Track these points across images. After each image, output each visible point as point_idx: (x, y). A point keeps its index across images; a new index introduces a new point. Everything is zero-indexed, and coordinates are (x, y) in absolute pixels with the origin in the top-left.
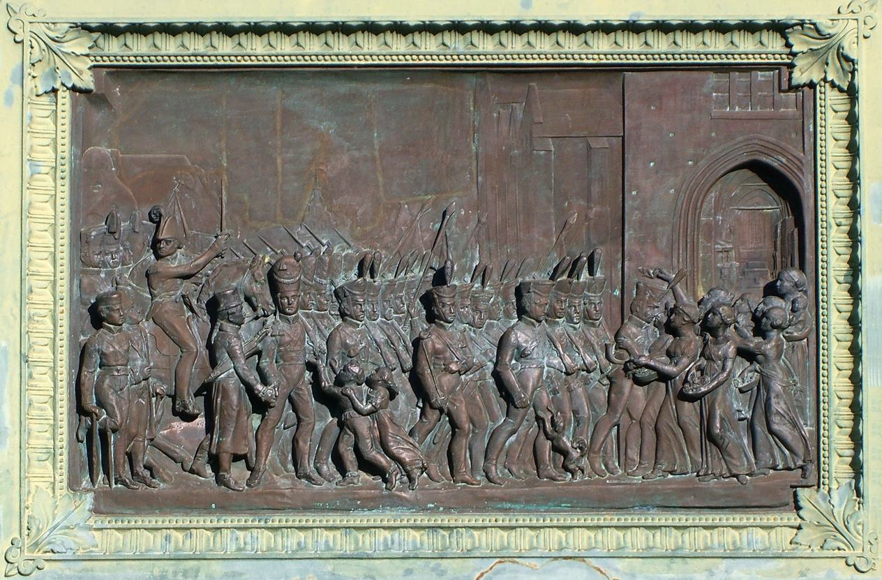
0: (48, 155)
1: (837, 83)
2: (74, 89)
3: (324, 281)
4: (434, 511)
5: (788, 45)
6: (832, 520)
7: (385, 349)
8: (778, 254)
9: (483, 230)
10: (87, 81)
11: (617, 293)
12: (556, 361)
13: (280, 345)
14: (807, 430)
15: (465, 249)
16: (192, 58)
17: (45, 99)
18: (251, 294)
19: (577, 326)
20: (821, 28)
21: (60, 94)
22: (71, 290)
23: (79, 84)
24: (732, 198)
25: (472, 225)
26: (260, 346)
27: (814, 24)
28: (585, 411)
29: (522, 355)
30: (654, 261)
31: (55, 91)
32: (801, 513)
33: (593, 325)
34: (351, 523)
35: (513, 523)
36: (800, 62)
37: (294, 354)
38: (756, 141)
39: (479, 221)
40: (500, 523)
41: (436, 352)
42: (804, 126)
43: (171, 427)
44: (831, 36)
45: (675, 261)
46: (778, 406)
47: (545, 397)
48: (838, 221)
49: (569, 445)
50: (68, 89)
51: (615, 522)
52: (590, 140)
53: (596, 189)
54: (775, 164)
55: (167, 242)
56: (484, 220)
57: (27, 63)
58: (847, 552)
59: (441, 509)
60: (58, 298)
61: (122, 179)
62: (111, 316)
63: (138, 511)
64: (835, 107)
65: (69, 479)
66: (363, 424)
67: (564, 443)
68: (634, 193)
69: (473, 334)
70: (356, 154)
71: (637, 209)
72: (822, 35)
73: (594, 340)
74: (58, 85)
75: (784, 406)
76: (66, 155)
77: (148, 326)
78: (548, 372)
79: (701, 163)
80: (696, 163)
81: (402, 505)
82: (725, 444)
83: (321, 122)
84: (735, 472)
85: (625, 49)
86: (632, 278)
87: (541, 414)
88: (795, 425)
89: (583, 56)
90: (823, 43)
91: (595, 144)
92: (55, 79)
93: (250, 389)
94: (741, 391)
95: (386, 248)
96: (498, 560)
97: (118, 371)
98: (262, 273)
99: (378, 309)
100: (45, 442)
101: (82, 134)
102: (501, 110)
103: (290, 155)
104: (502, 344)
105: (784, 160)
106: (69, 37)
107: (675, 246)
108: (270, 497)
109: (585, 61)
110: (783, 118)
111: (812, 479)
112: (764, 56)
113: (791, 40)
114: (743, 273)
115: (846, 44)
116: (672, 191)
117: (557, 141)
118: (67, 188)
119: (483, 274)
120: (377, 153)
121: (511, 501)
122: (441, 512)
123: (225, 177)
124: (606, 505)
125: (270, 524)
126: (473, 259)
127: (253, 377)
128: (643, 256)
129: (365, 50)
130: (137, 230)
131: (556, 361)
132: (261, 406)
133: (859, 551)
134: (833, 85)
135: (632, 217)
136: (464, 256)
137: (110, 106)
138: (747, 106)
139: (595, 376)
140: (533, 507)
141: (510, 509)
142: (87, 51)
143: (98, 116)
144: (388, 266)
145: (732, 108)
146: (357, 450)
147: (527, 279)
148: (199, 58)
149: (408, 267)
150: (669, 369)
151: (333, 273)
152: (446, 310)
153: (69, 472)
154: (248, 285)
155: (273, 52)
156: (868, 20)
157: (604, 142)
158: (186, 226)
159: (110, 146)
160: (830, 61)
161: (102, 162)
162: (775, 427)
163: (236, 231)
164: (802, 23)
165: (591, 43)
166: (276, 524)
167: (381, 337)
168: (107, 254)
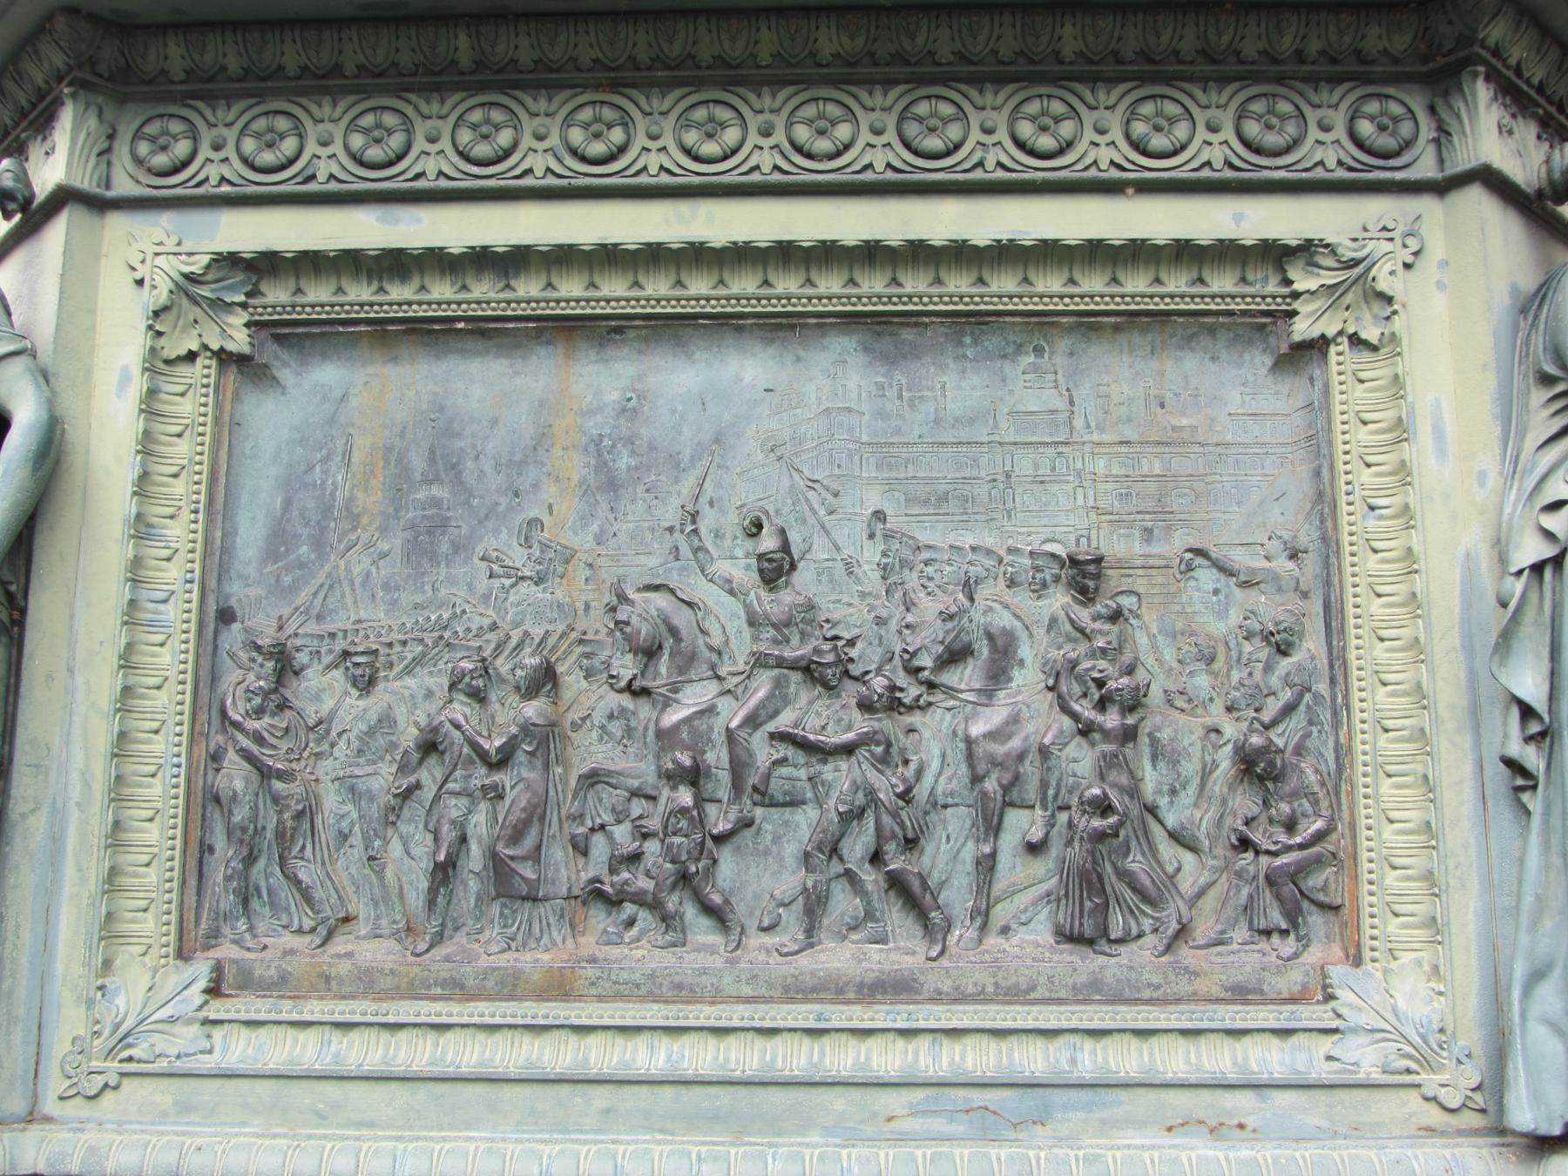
133: (1444, 1077)
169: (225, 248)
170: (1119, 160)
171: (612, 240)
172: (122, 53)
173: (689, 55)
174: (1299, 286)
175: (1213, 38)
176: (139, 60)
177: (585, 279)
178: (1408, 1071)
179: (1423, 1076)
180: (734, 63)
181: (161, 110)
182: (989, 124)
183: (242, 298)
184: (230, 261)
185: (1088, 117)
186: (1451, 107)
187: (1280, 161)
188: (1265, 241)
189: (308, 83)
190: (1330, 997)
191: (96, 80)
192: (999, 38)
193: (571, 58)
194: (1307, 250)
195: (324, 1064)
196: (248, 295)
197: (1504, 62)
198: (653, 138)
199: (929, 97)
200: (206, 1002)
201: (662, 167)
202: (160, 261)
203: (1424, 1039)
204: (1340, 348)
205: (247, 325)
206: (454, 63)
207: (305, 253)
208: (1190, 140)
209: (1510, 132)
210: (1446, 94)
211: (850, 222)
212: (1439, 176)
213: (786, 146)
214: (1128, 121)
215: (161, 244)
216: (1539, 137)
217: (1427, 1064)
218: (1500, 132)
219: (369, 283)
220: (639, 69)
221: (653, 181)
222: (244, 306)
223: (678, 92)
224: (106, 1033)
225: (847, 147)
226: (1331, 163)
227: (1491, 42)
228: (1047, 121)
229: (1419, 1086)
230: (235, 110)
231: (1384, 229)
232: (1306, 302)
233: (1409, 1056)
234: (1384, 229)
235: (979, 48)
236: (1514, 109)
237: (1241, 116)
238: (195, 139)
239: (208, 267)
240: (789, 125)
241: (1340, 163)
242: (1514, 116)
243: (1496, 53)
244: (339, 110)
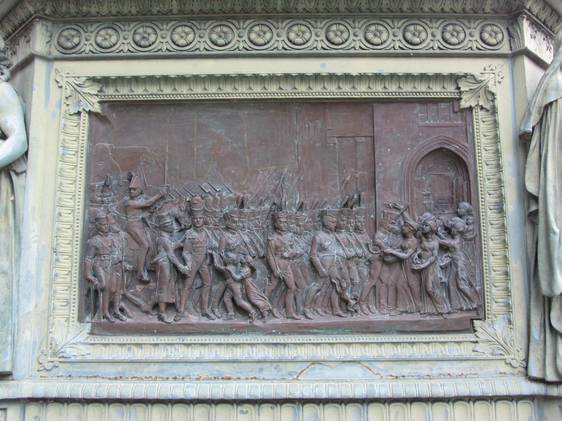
0: (74, 146)
1: (484, 106)
2: (90, 113)
3: (217, 210)
4: (276, 334)
5: (458, 88)
6: (496, 338)
7: (250, 246)
8: (454, 196)
9: (302, 184)
10: (97, 108)
11: (372, 216)
12: (341, 252)
13: (193, 244)
14: (478, 288)
15: (292, 194)
16: (151, 96)
17: (75, 117)
18: (178, 217)
19: (352, 234)
20: (476, 77)
21: (82, 115)
22: (84, 215)
23: (92, 110)
24: (429, 168)
25: (295, 182)
26: (182, 245)
27: (472, 76)
28: (357, 280)
29: (322, 248)
30: (391, 200)
31: (79, 113)
32: (477, 333)
33: (360, 233)
34: (230, 342)
35: (320, 341)
36: (464, 97)
37: (200, 249)
38: (442, 138)
39: (299, 179)
40: (312, 341)
41: (277, 248)
42: (467, 132)
43: (136, 288)
44: (481, 81)
45: (403, 199)
46: (463, 275)
47: (337, 274)
48: (489, 177)
49: (349, 297)
50: (87, 112)
51: (376, 341)
52: (356, 138)
53: (360, 163)
54: (453, 149)
55: (135, 189)
56: (301, 179)
57: (64, 97)
58: (506, 356)
59: (280, 333)
60: (75, 219)
61: (114, 159)
62: (101, 228)
63: (114, 334)
64: (483, 119)
65: (78, 316)
66: (237, 287)
67: (347, 296)
68: (380, 164)
69: (296, 238)
70: (235, 145)
71: (382, 173)
72: (476, 81)
73: (361, 241)
74: (81, 110)
75: (465, 275)
76: (85, 145)
77: (123, 234)
78: (337, 258)
79: (415, 149)
80: (412, 149)
81: (258, 331)
82: (435, 296)
83: (217, 129)
84: (440, 311)
85: (374, 90)
86: (380, 208)
87: (333, 281)
88: (471, 285)
89: (353, 94)
90: (477, 86)
91: (358, 140)
92: (79, 107)
93: (175, 267)
94: (441, 267)
95: (250, 193)
96: (311, 363)
97: (104, 257)
98: (184, 206)
99: (246, 225)
100: (65, 296)
101: (93, 137)
102: (310, 124)
103: (201, 146)
104: (313, 242)
105: (457, 147)
106: (86, 85)
107: (403, 191)
108: (186, 327)
109: (354, 96)
110: (457, 126)
111: (482, 316)
112: (445, 94)
113: (460, 85)
114: (436, 207)
115: (490, 85)
116: (400, 163)
117: (339, 139)
118: (84, 163)
119: (301, 207)
120: (246, 145)
121: (318, 329)
122: (280, 335)
123: (167, 157)
124: (370, 331)
125: (185, 342)
126: (296, 199)
127: (176, 261)
128: (386, 197)
129: (240, 91)
130: (121, 184)
131: (341, 252)
132: (182, 277)
133: (512, 356)
134: (482, 108)
135: (380, 177)
136: (292, 197)
137: (110, 123)
138: (437, 120)
139: (363, 260)
140: (330, 332)
141: (317, 333)
142: (96, 93)
143: (102, 128)
144: (252, 203)
145: (430, 121)
146: (233, 300)
147: (325, 209)
148: (154, 96)
149: (261, 203)
150: (402, 255)
151: (222, 206)
152: (282, 225)
153: (79, 312)
154: (177, 212)
155: (192, 92)
156: (500, 74)
157: (363, 139)
158: (146, 182)
159: (109, 142)
160: (481, 95)
161: (104, 150)
162: (461, 287)
163: (172, 184)
164: (465, 76)
165: (356, 87)
166: (189, 342)
167: (247, 239)
168: (105, 197)
169: (91, 75)
170: (402, 46)
171: (165, 74)
172: (53, 6)
173: (232, 9)
175: (350, 4)
176: (59, 8)
177: (129, 89)
178: (501, 354)
180: (206, 12)
181: (69, 27)
184: (94, 80)
185: (84, 35)
186: (514, 29)
188: (451, 74)
189: (202, 15)
190: (475, 331)
191: (45, 17)
192: (193, 5)
193: (232, 9)
195: (440, 355)
196: (98, 91)
197: (532, 13)
199: (336, 24)
200: (88, 337)
201: (244, 47)
202: (68, 80)
204: (477, 111)
206: (275, 9)
207: (119, 77)
209: (535, 37)
211: (309, 67)
214: (365, 33)
216: (544, 39)
218: (531, 38)
219: (261, 85)
220: (215, 13)
221: (163, 53)
222: (97, 95)
223: (288, 21)
227: (528, 7)
228: (183, 35)
229: (505, 359)
230: (285, 23)
231: (492, 70)
233: (500, 349)
234: (492, 70)
235: (311, 7)
236: (536, 29)
237: (327, 31)
241: (322, 47)
242: (536, 32)
243: (529, 10)
244: (206, 27)
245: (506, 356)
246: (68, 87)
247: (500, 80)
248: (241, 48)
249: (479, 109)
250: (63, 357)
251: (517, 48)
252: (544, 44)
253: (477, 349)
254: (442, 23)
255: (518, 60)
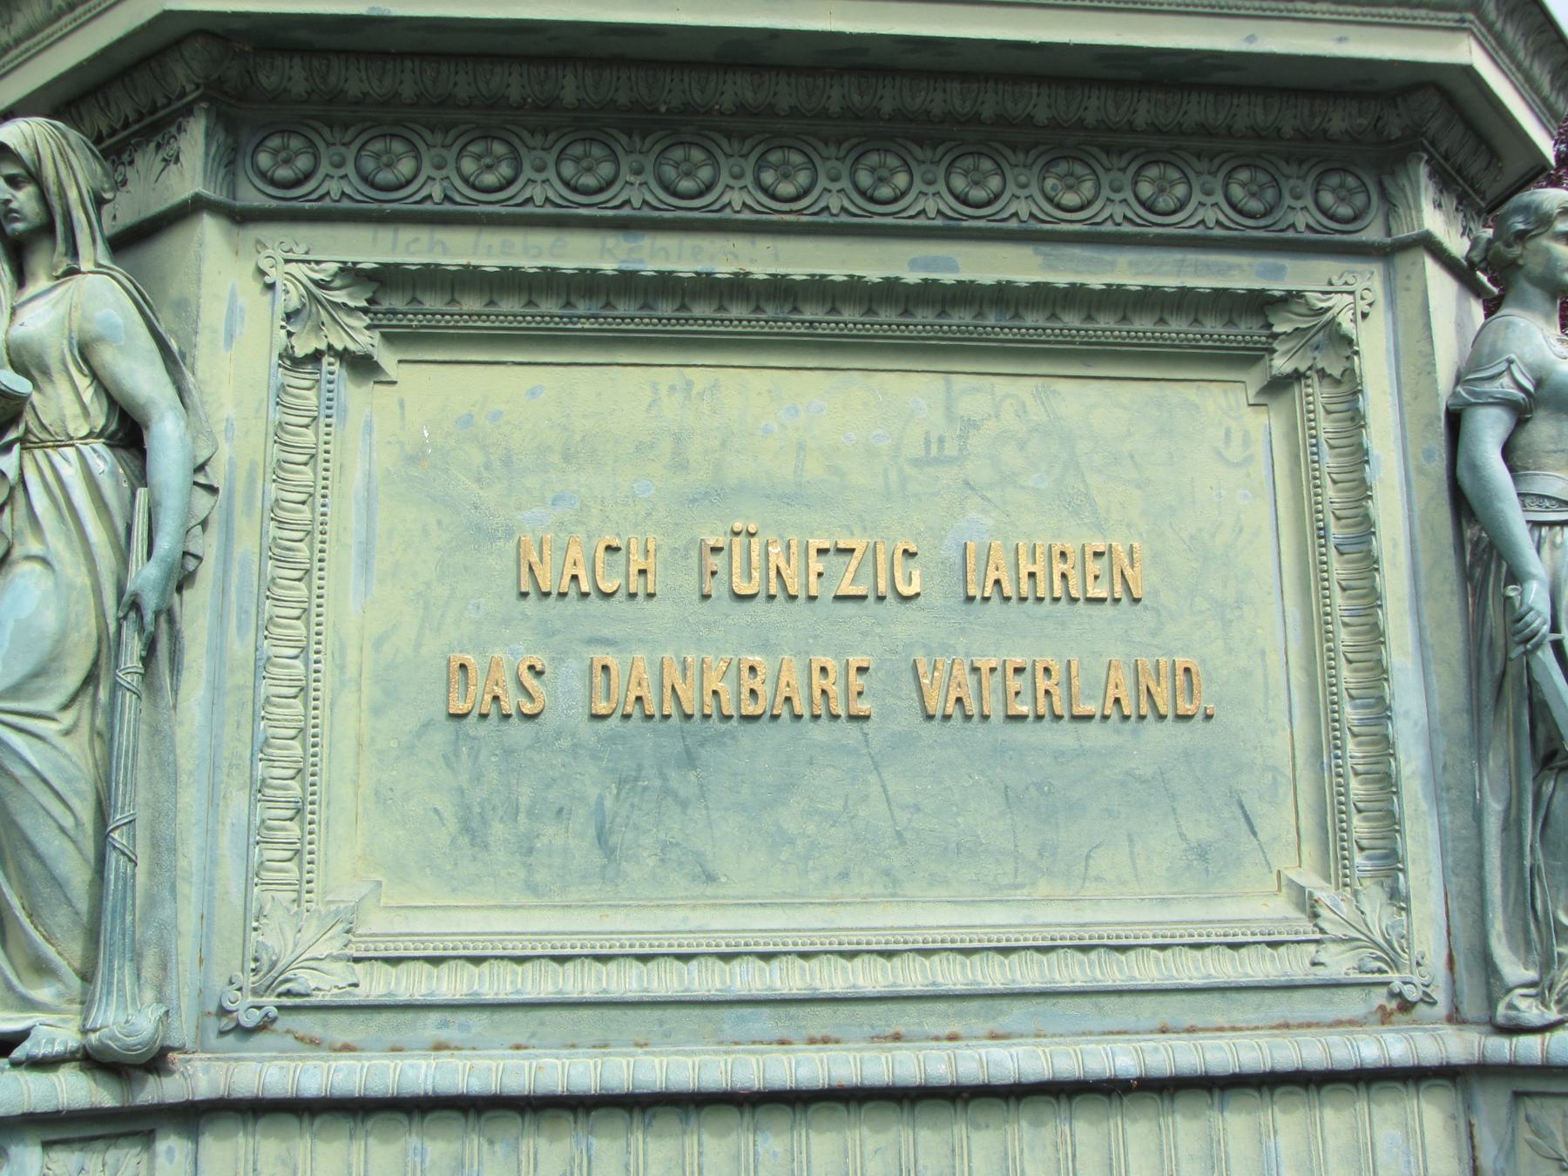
58: (1392, 976)
174: (1277, 329)
178: (1380, 971)
179: (1390, 974)
182: (1116, 184)
183: (365, 304)
184: (352, 275)
187: (1262, 223)
194: (1289, 299)
196: (368, 301)
198: (736, 177)
201: (744, 204)
203: (1389, 942)
205: (368, 328)
208: (415, 176)
210: (1392, 173)
212: (1389, 240)
213: (1132, 200)
214: (1317, 191)
215: (291, 250)
217: (1394, 964)
224: (265, 969)
225: (904, 194)
226: (1024, 215)
228: (1343, 193)
232: (1283, 341)
233: (1378, 958)
238: (317, 159)
239: (335, 275)
240: (1226, 186)
245: (1392, 976)
246: (290, 287)
247: (1366, 309)
248: (1119, 219)
249: (1316, 378)
250: (288, 993)
251: (1403, 232)
252: (1448, 222)
253: (1322, 958)
254: (1224, 162)
255: (1403, 261)
